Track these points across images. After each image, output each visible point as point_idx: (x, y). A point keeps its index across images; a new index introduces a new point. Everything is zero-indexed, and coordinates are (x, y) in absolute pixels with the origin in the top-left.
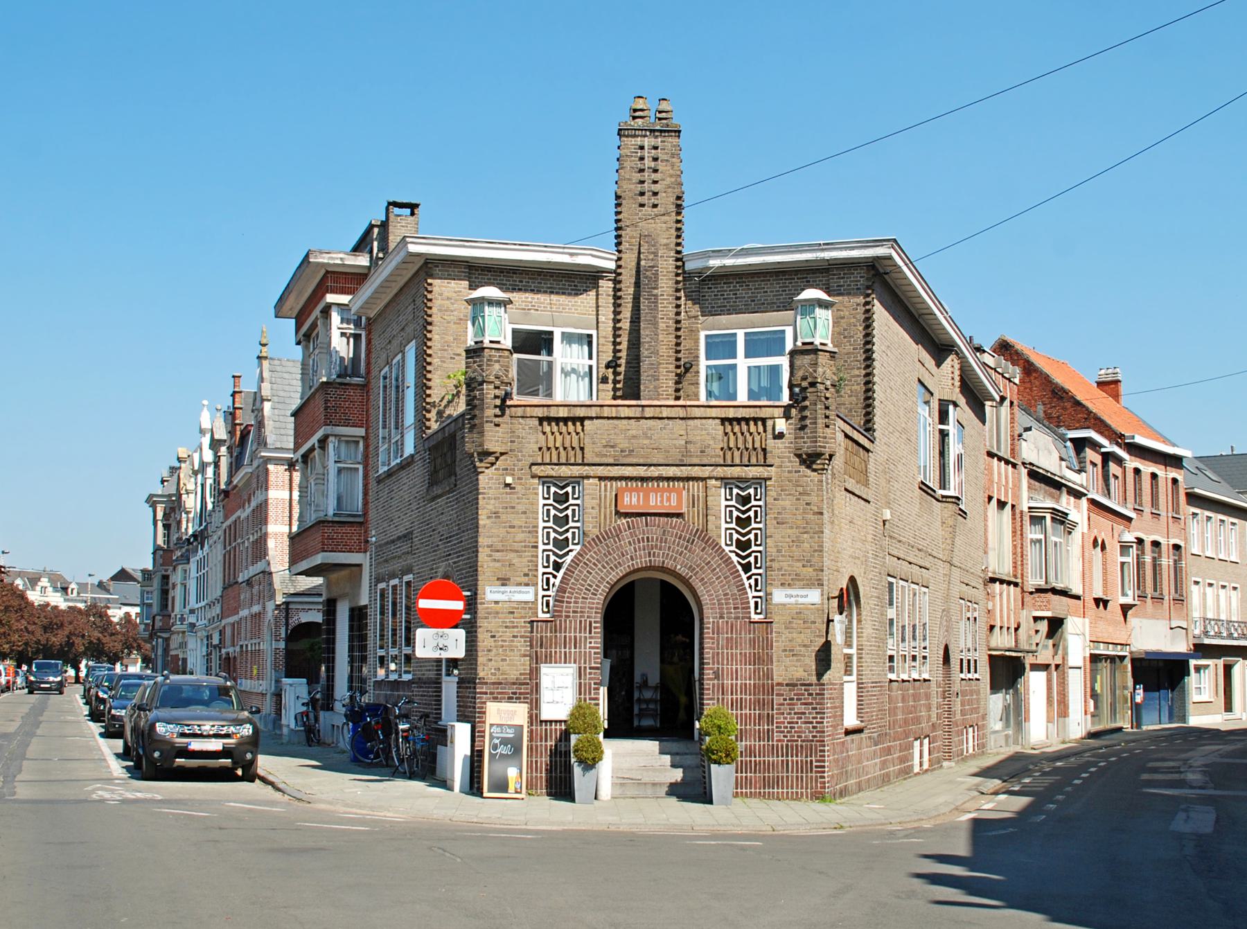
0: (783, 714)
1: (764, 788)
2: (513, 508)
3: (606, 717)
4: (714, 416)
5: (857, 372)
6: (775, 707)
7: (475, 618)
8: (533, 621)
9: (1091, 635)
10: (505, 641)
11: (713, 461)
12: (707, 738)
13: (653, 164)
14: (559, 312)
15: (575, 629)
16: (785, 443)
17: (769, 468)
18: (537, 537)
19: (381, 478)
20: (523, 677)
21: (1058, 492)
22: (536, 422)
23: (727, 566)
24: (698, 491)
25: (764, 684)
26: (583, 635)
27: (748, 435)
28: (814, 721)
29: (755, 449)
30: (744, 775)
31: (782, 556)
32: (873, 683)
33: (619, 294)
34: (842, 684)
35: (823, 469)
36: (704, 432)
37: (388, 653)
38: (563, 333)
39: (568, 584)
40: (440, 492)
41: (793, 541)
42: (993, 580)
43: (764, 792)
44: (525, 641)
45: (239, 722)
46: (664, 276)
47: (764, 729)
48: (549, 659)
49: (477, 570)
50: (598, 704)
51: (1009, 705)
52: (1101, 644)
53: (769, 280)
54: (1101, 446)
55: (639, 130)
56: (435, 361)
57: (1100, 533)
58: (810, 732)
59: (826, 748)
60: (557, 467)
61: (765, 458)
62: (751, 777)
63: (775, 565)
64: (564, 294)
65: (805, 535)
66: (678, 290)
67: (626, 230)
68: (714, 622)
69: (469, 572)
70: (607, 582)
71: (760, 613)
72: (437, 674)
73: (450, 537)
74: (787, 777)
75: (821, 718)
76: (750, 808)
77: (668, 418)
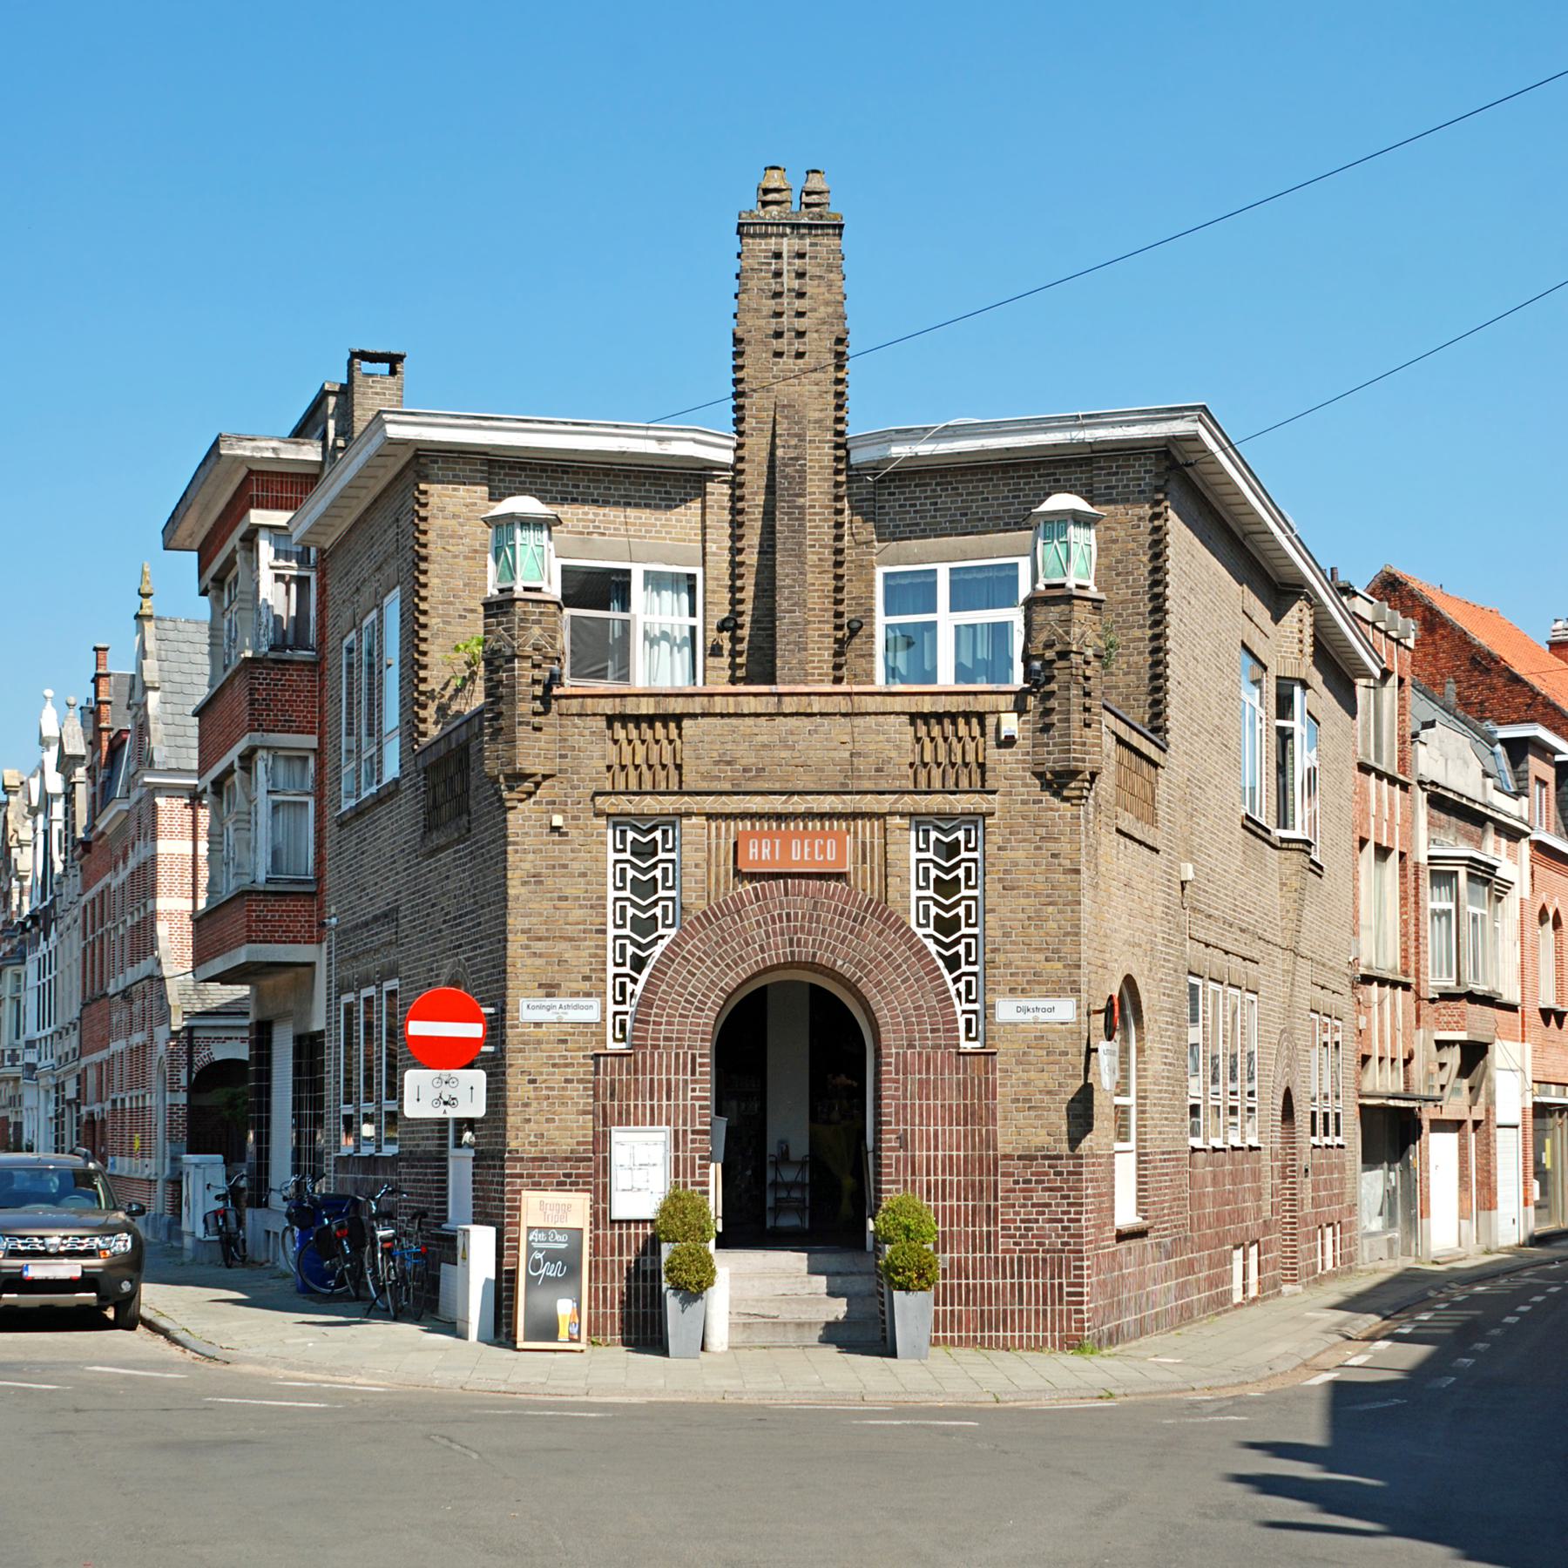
0: (1013, 1206)
1: (983, 1331)
2: (565, 866)
3: (720, 1213)
4: (898, 709)
5: (1137, 633)
6: (1000, 1194)
7: (502, 1051)
8: (598, 1055)
9: (1534, 1071)
10: (552, 1089)
11: (896, 785)
13: (796, 284)
14: (639, 537)
15: (668, 1067)
16: (1016, 754)
17: (990, 797)
18: (605, 915)
21: (1479, 830)
22: (603, 724)
23: (919, 960)
24: (872, 836)
25: (981, 1158)
26: (681, 1077)
27: (954, 741)
28: (1065, 1217)
29: (966, 765)
30: (949, 1308)
31: (1013, 943)
32: (1163, 1153)
33: (740, 505)
34: (1112, 1156)
35: (1080, 798)
36: (881, 737)
38: (647, 573)
39: (655, 993)
40: (443, 841)
42: (1367, 980)
44: (585, 1089)
45: (110, 1231)
46: (816, 474)
48: (625, 1119)
49: (505, 972)
50: (706, 1193)
51: (1395, 1189)
52: (1553, 1087)
53: (992, 479)
54: (1556, 752)
55: (772, 224)
56: (434, 622)
57: (1552, 898)
58: (1058, 1236)
59: (1086, 1263)
60: (637, 798)
61: (983, 780)
63: (1000, 958)
64: (647, 506)
65: (1050, 909)
66: (838, 498)
67: (751, 397)
68: (898, 1054)
69: (492, 975)
70: (722, 989)
71: (975, 1039)
72: (440, 1145)
73: (461, 916)
74: (1021, 1311)
75: (1077, 1213)
77: (822, 714)
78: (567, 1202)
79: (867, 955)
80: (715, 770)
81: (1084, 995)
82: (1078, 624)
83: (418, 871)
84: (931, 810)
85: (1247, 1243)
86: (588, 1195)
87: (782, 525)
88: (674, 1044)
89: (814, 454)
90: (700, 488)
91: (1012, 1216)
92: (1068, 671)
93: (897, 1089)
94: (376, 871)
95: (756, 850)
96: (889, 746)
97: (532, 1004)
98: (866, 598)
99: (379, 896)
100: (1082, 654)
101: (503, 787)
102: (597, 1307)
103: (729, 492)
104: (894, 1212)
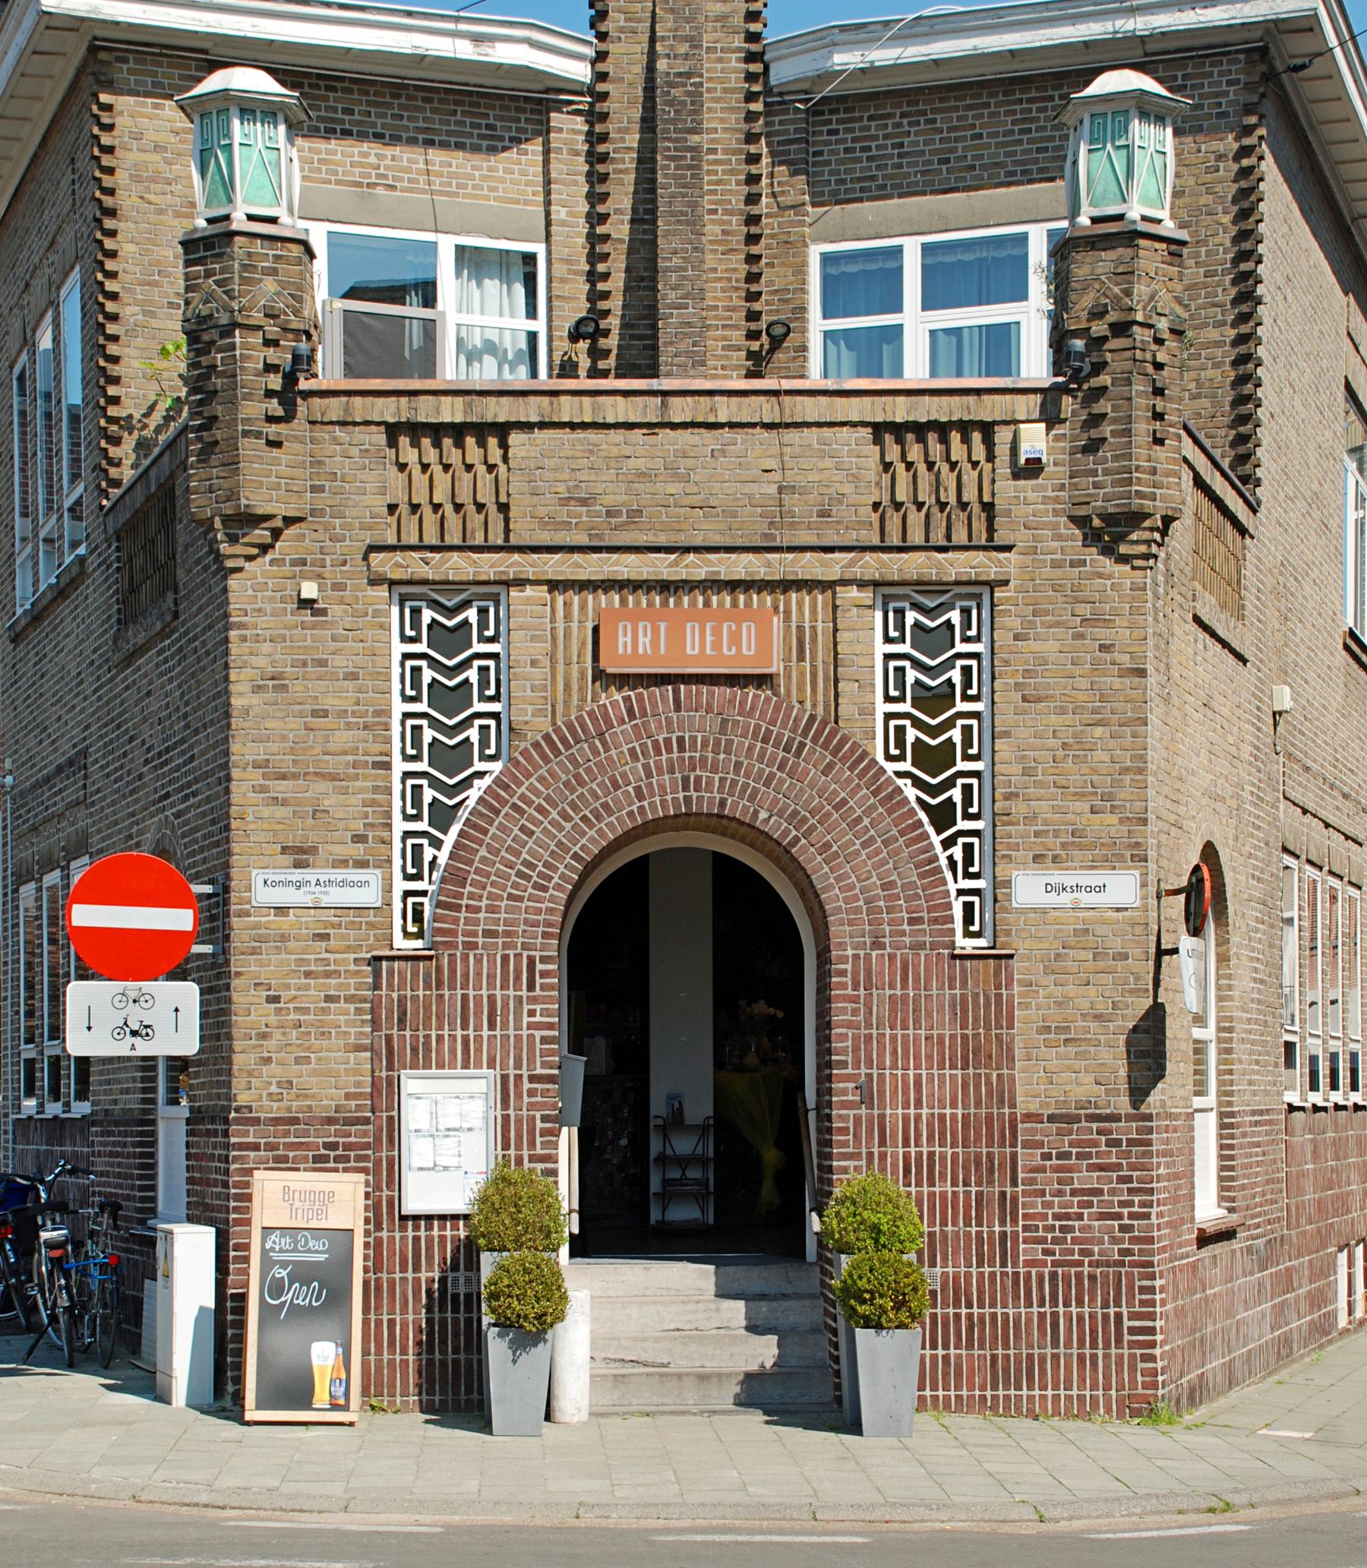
0: (1043, 1193)
1: (995, 1388)
2: (322, 663)
3: (576, 1206)
5: (1213, 334)
6: (1020, 1175)
7: (225, 951)
8: (378, 959)
11: (851, 538)
12: (845, 1260)
14: (448, 194)
15: (491, 977)
16: (1044, 488)
17: (1002, 556)
18: (388, 741)
19: (19, 629)
20: (353, 1103)
22: (382, 438)
23: (890, 812)
25: (989, 1118)
26: (511, 992)
27: (945, 468)
28: (1125, 1211)
29: (963, 506)
30: (940, 1352)
32: (1254, 1113)
33: (601, 148)
34: (1190, 1116)
35: (1146, 557)
36: (828, 463)
37: (42, 1054)
38: (460, 250)
40: (141, 639)
41: (1065, 746)
43: (995, 1398)
44: (358, 1011)
46: (718, 100)
47: (991, 1234)
48: (423, 1057)
49: (227, 828)
50: (554, 1173)
53: (987, 105)
56: (128, 311)
58: (1114, 1240)
59: (1158, 1283)
60: (438, 556)
61: (991, 530)
62: (959, 1357)
63: (1019, 808)
64: (460, 146)
65: (1098, 731)
66: (751, 138)
68: (856, 957)
69: (210, 835)
71: (978, 935)
72: (144, 1101)
73: (167, 750)
74: (1056, 1357)
75: (1143, 1204)
76: (963, 1446)
77: (732, 425)
78: (327, 1187)
79: (807, 802)
80: (563, 514)
81: (1152, 866)
82: (1145, 279)
83: (111, 689)
84: (907, 577)
85: (1353, 1242)
86: (362, 1177)
87: (666, 176)
88: (500, 941)
89: (715, 70)
90: (540, 122)
91: (1040, 1210)
92: (1128, 354)
93: (855, 1012)
94: (59, 701)
95: (629, 639)
96: (840, 476)
97: (271, 878)
98: (795, 291)
99: (63, 735)
100: (1151, 326)
101: (219, 536)
102: (379, 1351)
103: (586, 128)
104: (854, 1203)
